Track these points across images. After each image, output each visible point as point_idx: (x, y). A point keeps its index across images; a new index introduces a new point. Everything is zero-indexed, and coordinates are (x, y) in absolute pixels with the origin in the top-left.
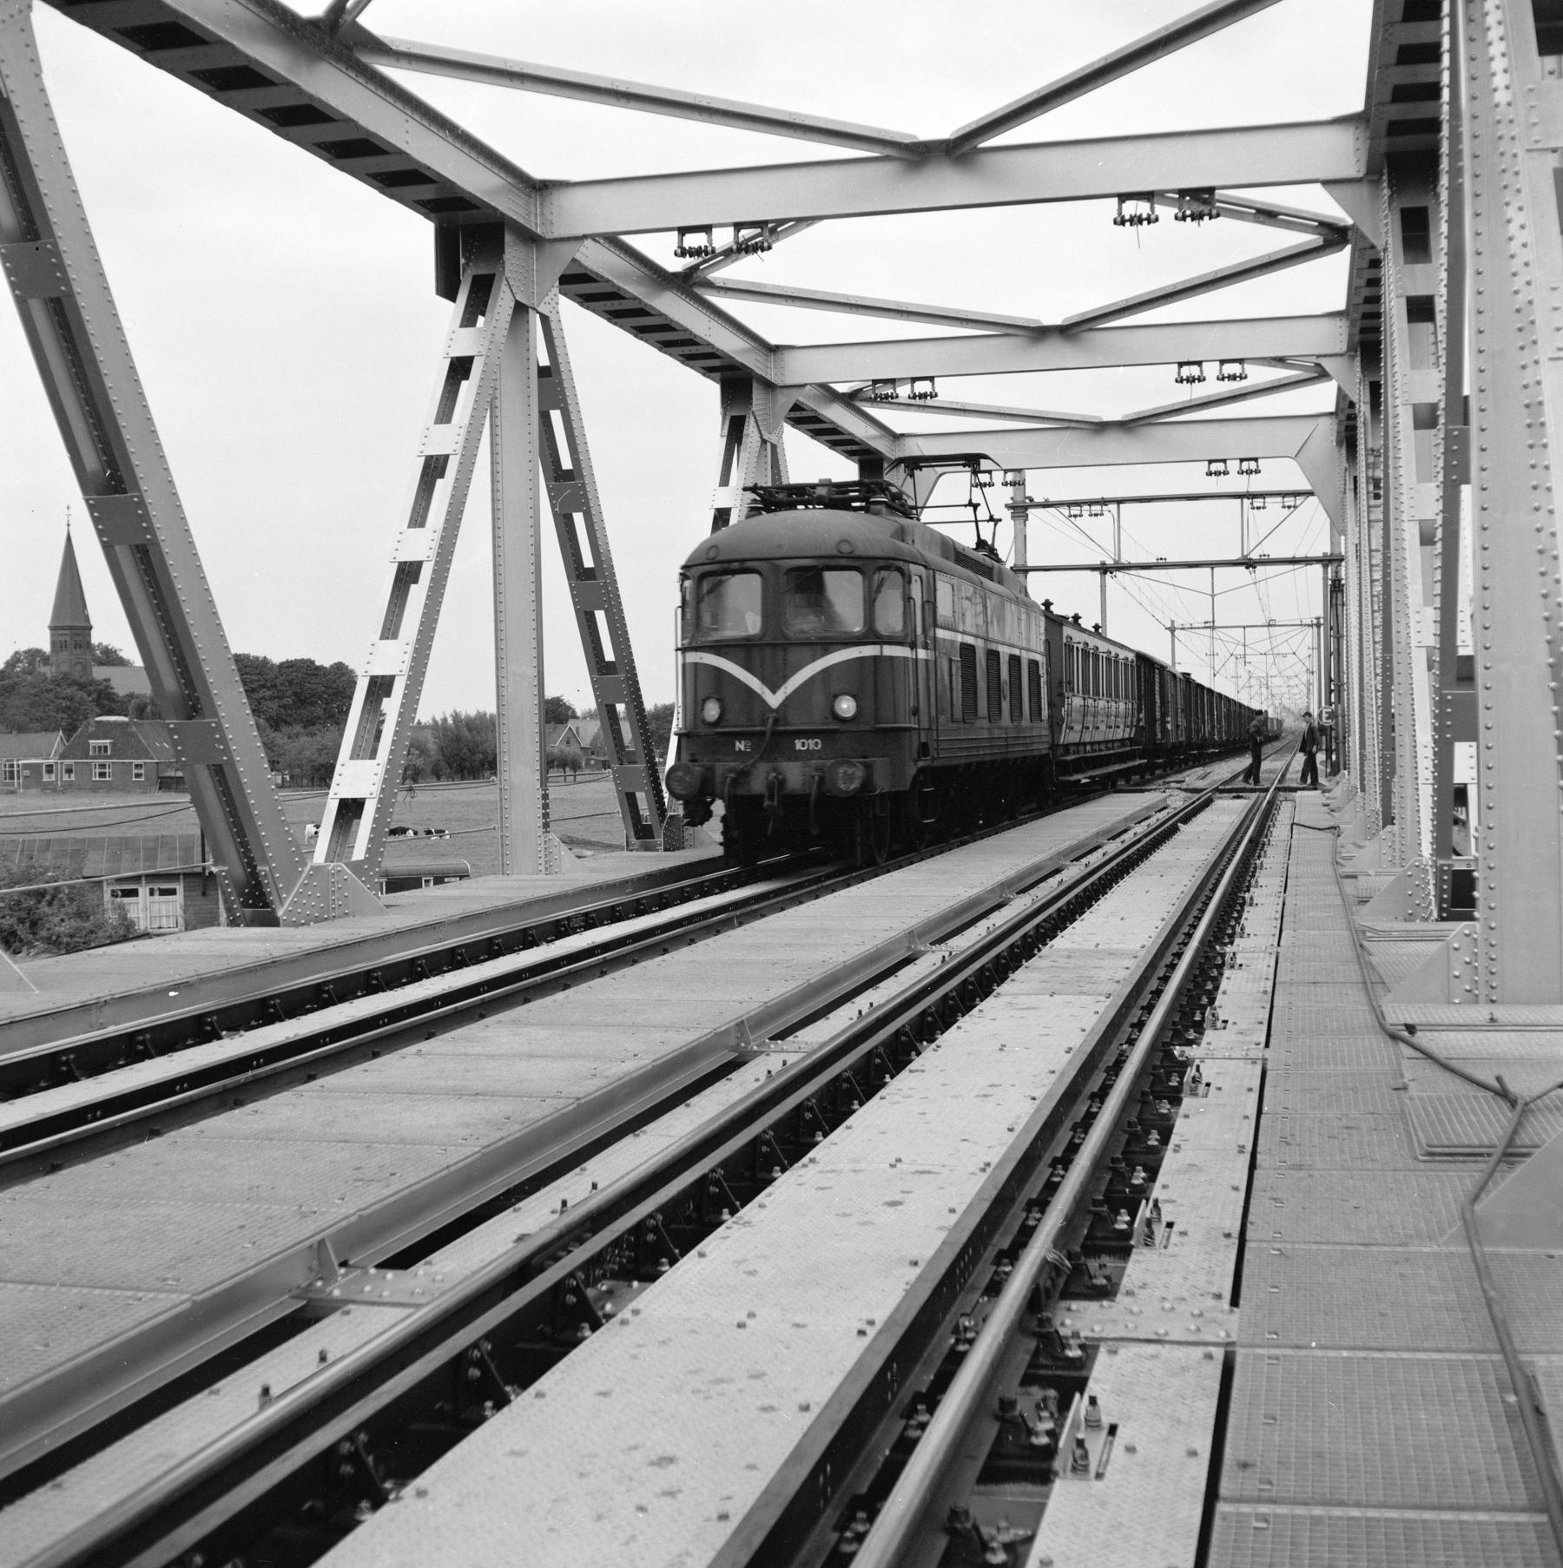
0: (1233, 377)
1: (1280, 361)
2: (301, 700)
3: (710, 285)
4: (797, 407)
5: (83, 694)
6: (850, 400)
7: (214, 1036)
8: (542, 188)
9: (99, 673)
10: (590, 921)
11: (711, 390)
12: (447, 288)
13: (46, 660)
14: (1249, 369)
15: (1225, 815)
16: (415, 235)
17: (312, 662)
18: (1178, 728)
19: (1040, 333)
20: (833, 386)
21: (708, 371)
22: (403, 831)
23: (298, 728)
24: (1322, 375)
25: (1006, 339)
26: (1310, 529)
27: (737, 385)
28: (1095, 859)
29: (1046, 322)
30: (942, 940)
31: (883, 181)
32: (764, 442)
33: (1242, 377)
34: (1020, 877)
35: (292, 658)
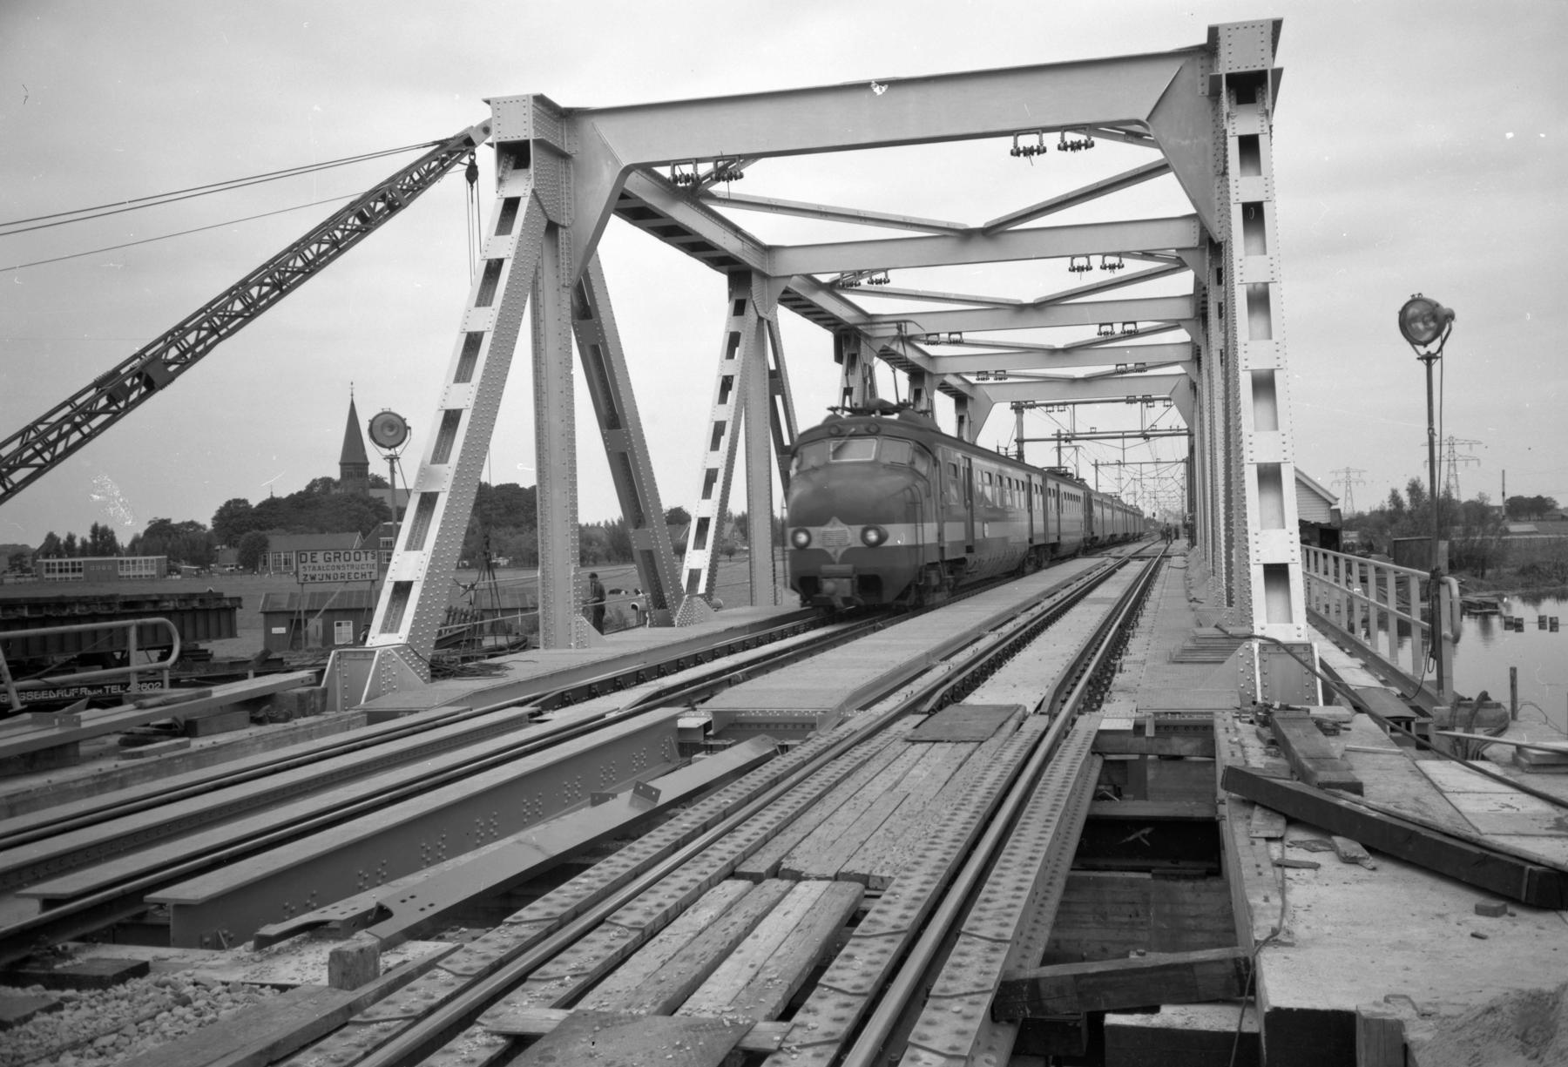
0: (1112, 267)
1: (1147, 255)
2: (511, 510)
3: (712, 197)
4: (786, 291)
5: (364, 508)
6: (831, 288)
7: (701, 662)
8: (769, 250)
9: (375, 493)
10: (730, 650)
11: (718, 282)
12: (839, 359)
13: (337, 484)
14: (1125, 261)
15: (1135, 567)
16: (826, 338)
17: (516, 486)
18: (1107, 536)
19: (1021, 308)
20: (818, 277)
21: (826, 326)
22: (618, 591)
23: (511, 529)
24: (1181, 265)
25: (941, 241)
26: (1172, 418)
27: (740, 276)
28: (1037, 610)
29: (972, 226)
30: (946, 658)
31: (947, 245)
32: (760, 319)
33: (1120, 266)
34: (1024, 604)
35: (504, 482)
